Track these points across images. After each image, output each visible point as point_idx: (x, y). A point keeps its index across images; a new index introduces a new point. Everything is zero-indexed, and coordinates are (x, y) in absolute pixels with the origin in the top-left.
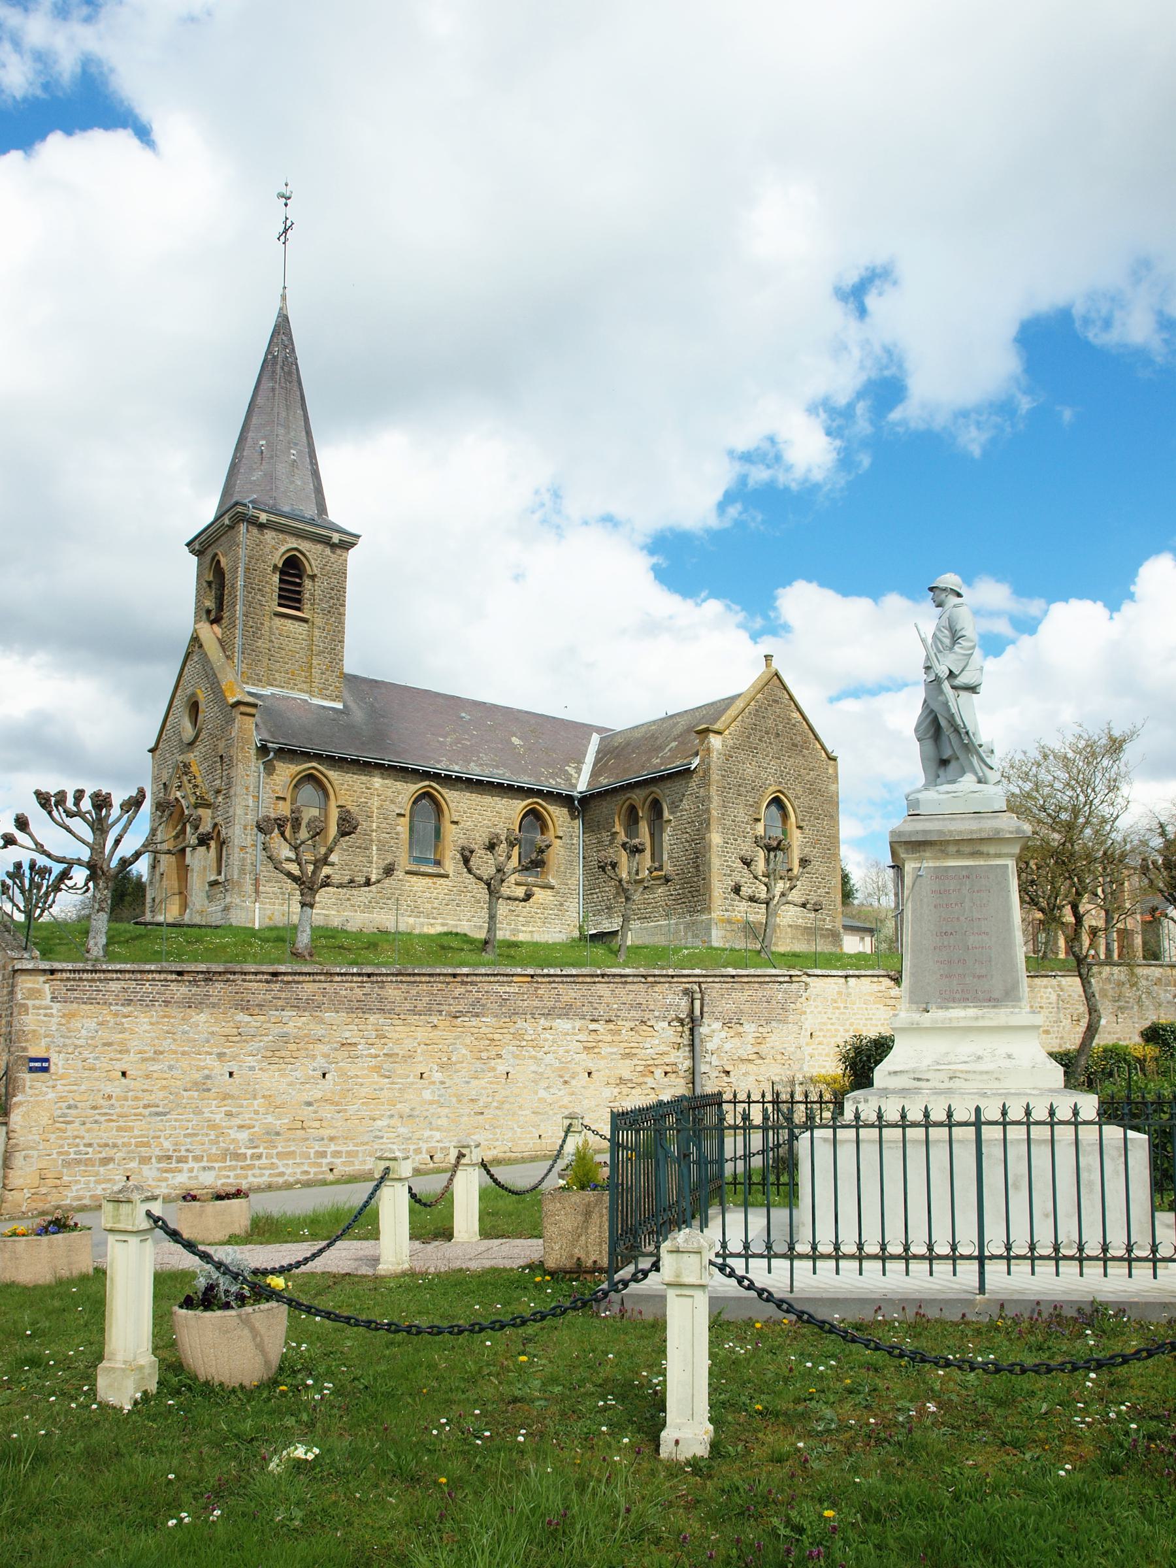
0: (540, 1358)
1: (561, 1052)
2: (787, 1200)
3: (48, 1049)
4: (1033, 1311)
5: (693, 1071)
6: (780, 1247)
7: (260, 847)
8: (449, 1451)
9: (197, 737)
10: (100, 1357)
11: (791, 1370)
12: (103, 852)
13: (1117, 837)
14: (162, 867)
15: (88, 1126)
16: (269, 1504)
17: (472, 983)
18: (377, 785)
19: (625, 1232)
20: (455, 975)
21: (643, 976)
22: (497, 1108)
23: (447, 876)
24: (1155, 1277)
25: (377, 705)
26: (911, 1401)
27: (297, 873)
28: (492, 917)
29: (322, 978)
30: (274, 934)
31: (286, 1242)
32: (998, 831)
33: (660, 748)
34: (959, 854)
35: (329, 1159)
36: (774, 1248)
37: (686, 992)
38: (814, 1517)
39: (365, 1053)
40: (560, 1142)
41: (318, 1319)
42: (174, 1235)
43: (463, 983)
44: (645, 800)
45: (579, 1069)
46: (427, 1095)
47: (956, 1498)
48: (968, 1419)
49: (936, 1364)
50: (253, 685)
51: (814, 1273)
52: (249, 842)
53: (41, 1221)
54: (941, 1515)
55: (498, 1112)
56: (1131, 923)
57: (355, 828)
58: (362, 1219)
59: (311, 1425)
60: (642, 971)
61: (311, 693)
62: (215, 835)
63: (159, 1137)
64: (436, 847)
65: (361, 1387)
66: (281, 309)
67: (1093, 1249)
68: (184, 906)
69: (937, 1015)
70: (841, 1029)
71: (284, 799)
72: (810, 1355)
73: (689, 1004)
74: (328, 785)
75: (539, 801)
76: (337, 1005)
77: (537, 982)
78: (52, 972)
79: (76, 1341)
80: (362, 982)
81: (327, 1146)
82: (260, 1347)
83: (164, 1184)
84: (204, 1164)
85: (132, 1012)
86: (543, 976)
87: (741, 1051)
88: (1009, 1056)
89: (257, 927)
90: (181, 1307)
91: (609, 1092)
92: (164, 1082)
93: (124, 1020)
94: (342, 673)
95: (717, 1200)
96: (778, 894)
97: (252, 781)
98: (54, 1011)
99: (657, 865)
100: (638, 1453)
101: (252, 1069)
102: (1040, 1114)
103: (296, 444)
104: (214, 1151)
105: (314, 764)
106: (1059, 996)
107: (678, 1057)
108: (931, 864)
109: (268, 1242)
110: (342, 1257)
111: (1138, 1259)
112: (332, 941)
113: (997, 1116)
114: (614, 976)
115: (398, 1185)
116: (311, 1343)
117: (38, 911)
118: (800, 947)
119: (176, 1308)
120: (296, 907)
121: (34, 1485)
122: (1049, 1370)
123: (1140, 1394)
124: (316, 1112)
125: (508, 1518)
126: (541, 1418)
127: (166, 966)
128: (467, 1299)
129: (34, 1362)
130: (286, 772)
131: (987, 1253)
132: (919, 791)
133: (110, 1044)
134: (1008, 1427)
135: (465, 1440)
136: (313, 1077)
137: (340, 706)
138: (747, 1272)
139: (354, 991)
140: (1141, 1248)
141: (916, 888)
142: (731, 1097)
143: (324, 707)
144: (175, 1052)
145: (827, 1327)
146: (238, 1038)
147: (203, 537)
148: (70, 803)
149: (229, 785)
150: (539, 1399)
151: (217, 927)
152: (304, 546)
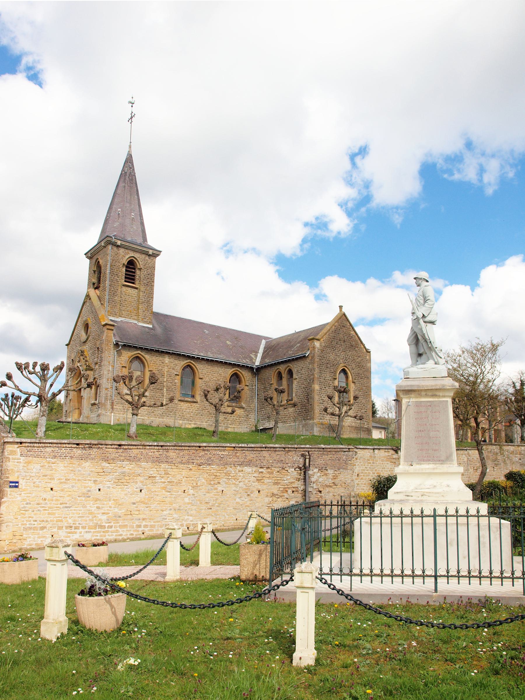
0: (238, 620)
1: (246, 481)
2: (350, 550)
3: (18, 477)
4: (459, 600)
5: (305, 491)
6: (346, 571)
7: (114, 388)
8: (198, 661)
9: (87, 339)
10: (42, 617)
11: (351, 626)
12: (45, 390)
13: (495, 388)
14: (70, 397)
15: (35, 512)
16: (118, 685)
17: (207, 450)
18: (167, 362)
19: (277, 563)
20: (200, 447)
21: (283, 448)
22: (218, 506)
23: (197, 402)
24: (513, 586)
25: (167, 326)
26: (405, 641)
27: (131, 400)
28: (217, 421)
29: (141, 447)
30: (120, 427)
31: (124, 566)
32: (444, 386)
33: (292, 346)
34: (426, 396)
35: (142, 528)
36: (384, 571)
37: (303, 455)
38: (363, 693)
39: (159, 481)
40: (247, 522)
41: (139, 601)
42: (77, 563)
43: (204, 450)
44: (285, 370)
45: (255, 489)
46: (187, 500)
47: (426, 685)
48: (431, 650)
49: (417, 624)
50: (113, 316)
51: (361, 582)
52: (109, 386)
53: (14, 555)
54: (419, 693)
55: (218, 508)
56: (500, 427)
57: (157, 380)
58: (159, 556)
59: (137, 649)
60: (283, 446)
61: (138, 320)
62: (94, 383)
63: (67, 518)
64: (192, 389)
65: (159, 632)
66: (129, 152)
67: (485, 573)
68: (80, 414)
69: (416, 467)
70: (371, 472)
71: (125, 367)
72: (359, 619)
73: (304, 461)
74: (145, 361)
75: (239, 369)
76: (147, 459)
77: (236, 450)
78: (21, 443)
79: (31, 610)
80: (159, 449)
81: (141, 522)
82: (114, 613)
83: (68, 539)
84: (87, 530)
85: (56, 461)
86: (239, 447)
87: (326, 482)
88: (448, 486)
89: (112, 424)
90: (79, 595)
91: (267, 500)
92: (70, 493)
93: (52, 465)
94: (152, 312)
95: (317, 549)
96: (344, 412)
97: (111, 359)
98: (21, 461)
99: (290, 398)
100: (283, 663)
101: (109, 487)
102: (462, 512)
103: (134, 211)
104: (91, 524)
105: (139, 352)
106: (468, 458)
107: (299, 484)
108: (414, 400)
109: (116, 566)
110: (150, 573)
111: (506, 578)
112: (146, 430)
113: (443, 513)
114: (271, 448)
115: (175, 540)
116: (136, 612)
117: (15, 416)
118: (353, 436)
119: (77, 595)
120: (130, 416)
121: (13, 675)
122: (467, 627)
123: (507, 639)
124: (137, 507)
125: (225, 692)
126: (239, 647)
127: (71, 441)
128: (206, 592)
129: (12, 619)
130: (127, 355)
131: (438, 574)
132: (409, 368)
133: (46, 476)
134: (448, 653)
135: (205, 656)
136: (136, 492)
137: (151, 326)
138: (331, 581)
139: (155, 453)
140: (507, 572)
141: (407, 411)
142: (362, 503)
143: (144, 327)
144: (75, 480)
145: (368, 607)
146: (103, 474)
147: (92, 251)
148: (31, 368)
149: (101, 361)
150: (238, 638)
151: (95, 424)
152: (137, 255)
